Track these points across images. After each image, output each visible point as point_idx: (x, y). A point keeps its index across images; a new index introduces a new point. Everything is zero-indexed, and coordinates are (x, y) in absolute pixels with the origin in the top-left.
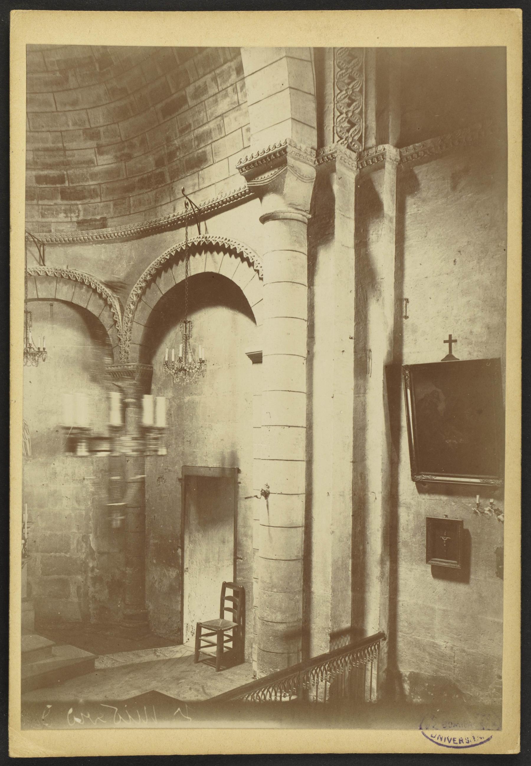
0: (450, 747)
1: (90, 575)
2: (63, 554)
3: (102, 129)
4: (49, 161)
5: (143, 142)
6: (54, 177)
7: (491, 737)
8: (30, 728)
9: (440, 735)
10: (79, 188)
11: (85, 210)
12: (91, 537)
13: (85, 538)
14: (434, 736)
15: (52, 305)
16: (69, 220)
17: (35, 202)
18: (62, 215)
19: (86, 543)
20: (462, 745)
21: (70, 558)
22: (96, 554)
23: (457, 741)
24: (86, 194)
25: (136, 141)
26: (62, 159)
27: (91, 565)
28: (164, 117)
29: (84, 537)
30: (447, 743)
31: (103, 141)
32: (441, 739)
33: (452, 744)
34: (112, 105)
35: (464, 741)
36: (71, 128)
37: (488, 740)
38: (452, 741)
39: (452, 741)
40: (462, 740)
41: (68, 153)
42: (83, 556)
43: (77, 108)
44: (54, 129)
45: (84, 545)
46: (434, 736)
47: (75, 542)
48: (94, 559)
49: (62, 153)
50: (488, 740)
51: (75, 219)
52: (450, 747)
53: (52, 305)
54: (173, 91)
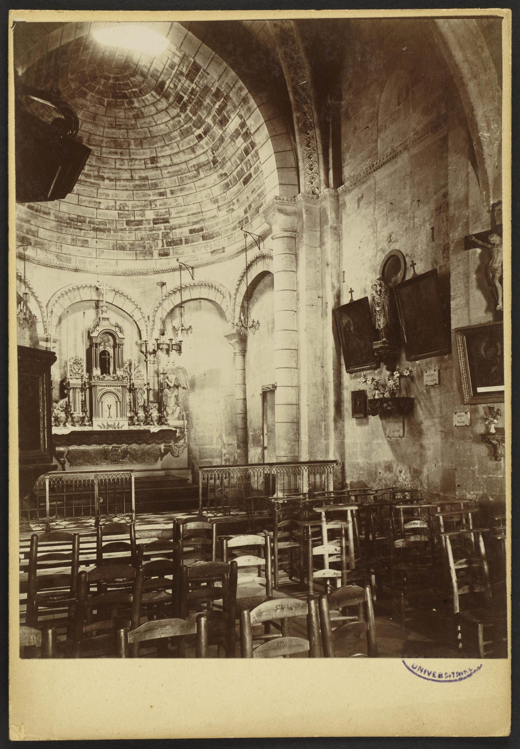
0: (429, 679)
1: (224, 458)
2: (209, 446)
3: (219, 197)
4: (195, 220)
5: (238, 201)
6: (198, 229)
7: (481, 665)
8: (351, 394)
9: (420, 667)
10: (211, 233)
11: (214, 244)
12: (224, 435)
13: (220, 437)
14: (415, 666)
15: (200, 302)
16: (206, 251)
17: (189, 244)
18: (203, 249)
19: (221, 439)
20: (441, 679)
21: (213, 449)
22: (226, 446)
23: (437, 675)
24: (214, 235)
25: (235, 201)
26: (201, 217)
27: (224, 452)
28: (244, 185)
29: (220, 436)
30: (426, 676)
31: (220, 204)
32: (422, 671)
33: (431, 677)
34: (222, 183)
35: (444, 676)
36: (204, 199)
37: (479, 668)
38: (431, 675)
39: (431, 675)
40: (441, 675)
41: (204, 214)
42: (220, 447)
43: (206, 188)
44: (196, 202)
45: (220, 440)
46: (415, 666)
47: (216, 439)
48: (225, 448)
49: (201, 214)
50: (479, 668)
51: (210, 251)
52: (429, 679)
53: (200, 302)
54: (246, 171)
